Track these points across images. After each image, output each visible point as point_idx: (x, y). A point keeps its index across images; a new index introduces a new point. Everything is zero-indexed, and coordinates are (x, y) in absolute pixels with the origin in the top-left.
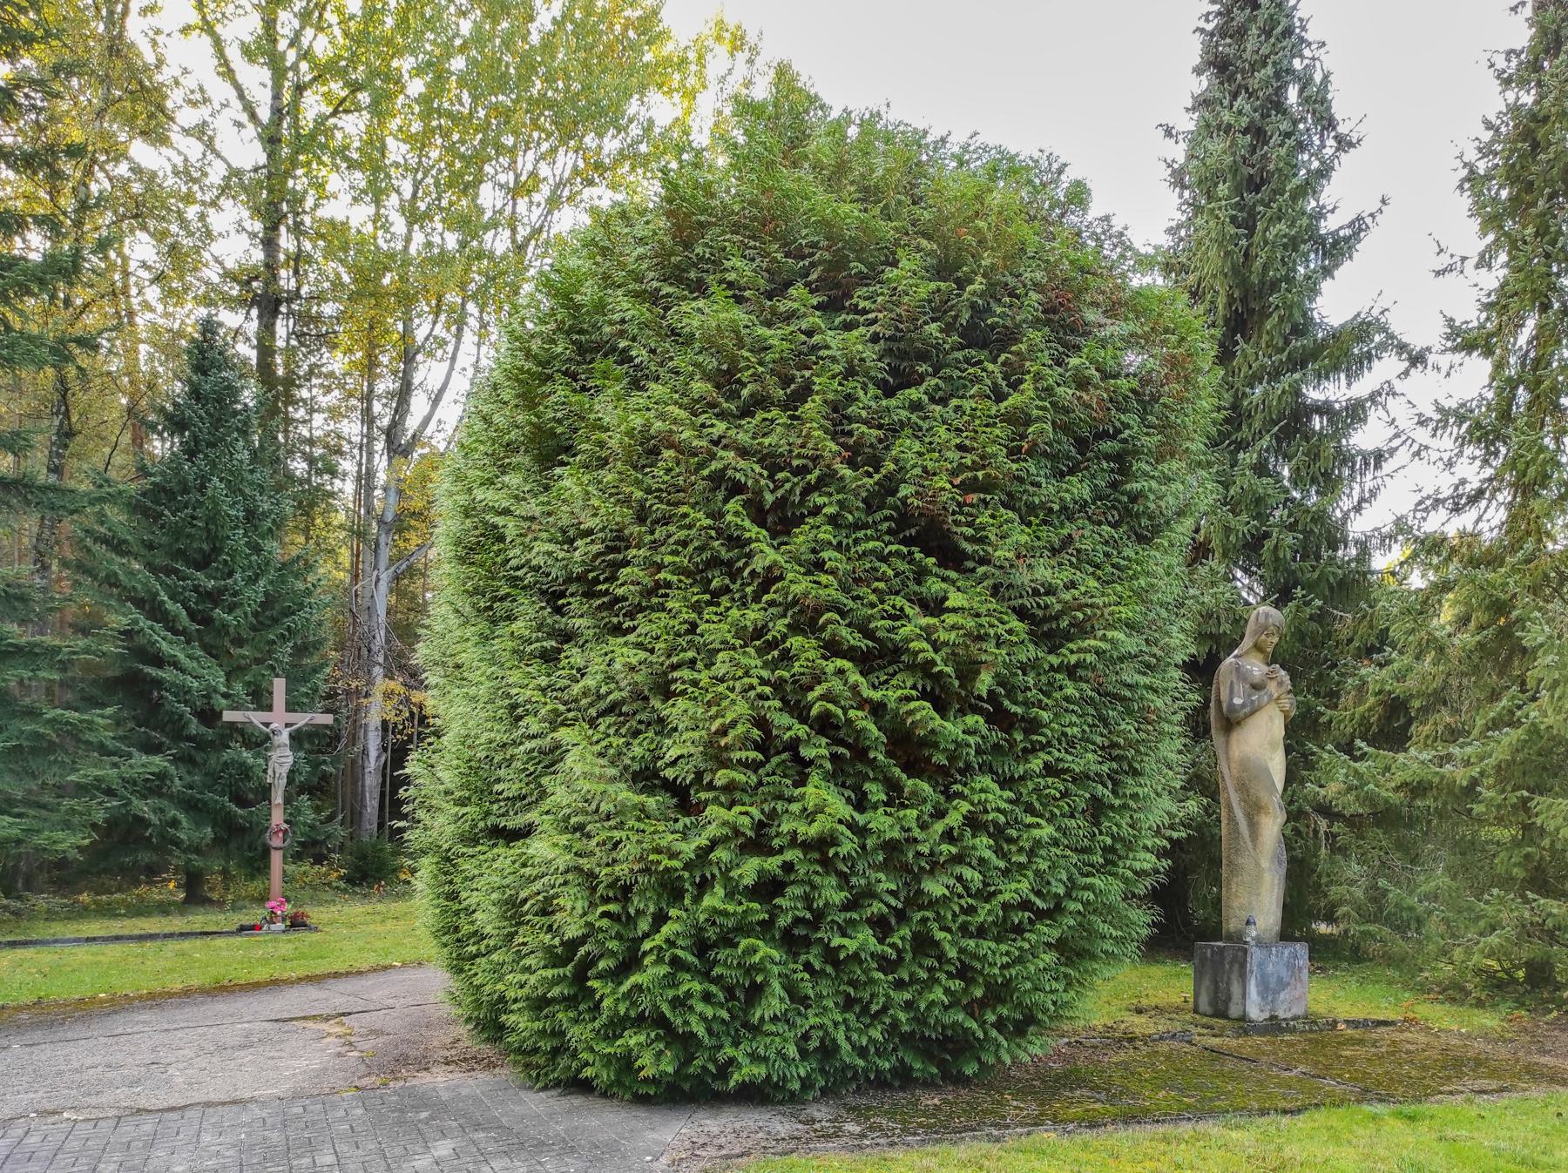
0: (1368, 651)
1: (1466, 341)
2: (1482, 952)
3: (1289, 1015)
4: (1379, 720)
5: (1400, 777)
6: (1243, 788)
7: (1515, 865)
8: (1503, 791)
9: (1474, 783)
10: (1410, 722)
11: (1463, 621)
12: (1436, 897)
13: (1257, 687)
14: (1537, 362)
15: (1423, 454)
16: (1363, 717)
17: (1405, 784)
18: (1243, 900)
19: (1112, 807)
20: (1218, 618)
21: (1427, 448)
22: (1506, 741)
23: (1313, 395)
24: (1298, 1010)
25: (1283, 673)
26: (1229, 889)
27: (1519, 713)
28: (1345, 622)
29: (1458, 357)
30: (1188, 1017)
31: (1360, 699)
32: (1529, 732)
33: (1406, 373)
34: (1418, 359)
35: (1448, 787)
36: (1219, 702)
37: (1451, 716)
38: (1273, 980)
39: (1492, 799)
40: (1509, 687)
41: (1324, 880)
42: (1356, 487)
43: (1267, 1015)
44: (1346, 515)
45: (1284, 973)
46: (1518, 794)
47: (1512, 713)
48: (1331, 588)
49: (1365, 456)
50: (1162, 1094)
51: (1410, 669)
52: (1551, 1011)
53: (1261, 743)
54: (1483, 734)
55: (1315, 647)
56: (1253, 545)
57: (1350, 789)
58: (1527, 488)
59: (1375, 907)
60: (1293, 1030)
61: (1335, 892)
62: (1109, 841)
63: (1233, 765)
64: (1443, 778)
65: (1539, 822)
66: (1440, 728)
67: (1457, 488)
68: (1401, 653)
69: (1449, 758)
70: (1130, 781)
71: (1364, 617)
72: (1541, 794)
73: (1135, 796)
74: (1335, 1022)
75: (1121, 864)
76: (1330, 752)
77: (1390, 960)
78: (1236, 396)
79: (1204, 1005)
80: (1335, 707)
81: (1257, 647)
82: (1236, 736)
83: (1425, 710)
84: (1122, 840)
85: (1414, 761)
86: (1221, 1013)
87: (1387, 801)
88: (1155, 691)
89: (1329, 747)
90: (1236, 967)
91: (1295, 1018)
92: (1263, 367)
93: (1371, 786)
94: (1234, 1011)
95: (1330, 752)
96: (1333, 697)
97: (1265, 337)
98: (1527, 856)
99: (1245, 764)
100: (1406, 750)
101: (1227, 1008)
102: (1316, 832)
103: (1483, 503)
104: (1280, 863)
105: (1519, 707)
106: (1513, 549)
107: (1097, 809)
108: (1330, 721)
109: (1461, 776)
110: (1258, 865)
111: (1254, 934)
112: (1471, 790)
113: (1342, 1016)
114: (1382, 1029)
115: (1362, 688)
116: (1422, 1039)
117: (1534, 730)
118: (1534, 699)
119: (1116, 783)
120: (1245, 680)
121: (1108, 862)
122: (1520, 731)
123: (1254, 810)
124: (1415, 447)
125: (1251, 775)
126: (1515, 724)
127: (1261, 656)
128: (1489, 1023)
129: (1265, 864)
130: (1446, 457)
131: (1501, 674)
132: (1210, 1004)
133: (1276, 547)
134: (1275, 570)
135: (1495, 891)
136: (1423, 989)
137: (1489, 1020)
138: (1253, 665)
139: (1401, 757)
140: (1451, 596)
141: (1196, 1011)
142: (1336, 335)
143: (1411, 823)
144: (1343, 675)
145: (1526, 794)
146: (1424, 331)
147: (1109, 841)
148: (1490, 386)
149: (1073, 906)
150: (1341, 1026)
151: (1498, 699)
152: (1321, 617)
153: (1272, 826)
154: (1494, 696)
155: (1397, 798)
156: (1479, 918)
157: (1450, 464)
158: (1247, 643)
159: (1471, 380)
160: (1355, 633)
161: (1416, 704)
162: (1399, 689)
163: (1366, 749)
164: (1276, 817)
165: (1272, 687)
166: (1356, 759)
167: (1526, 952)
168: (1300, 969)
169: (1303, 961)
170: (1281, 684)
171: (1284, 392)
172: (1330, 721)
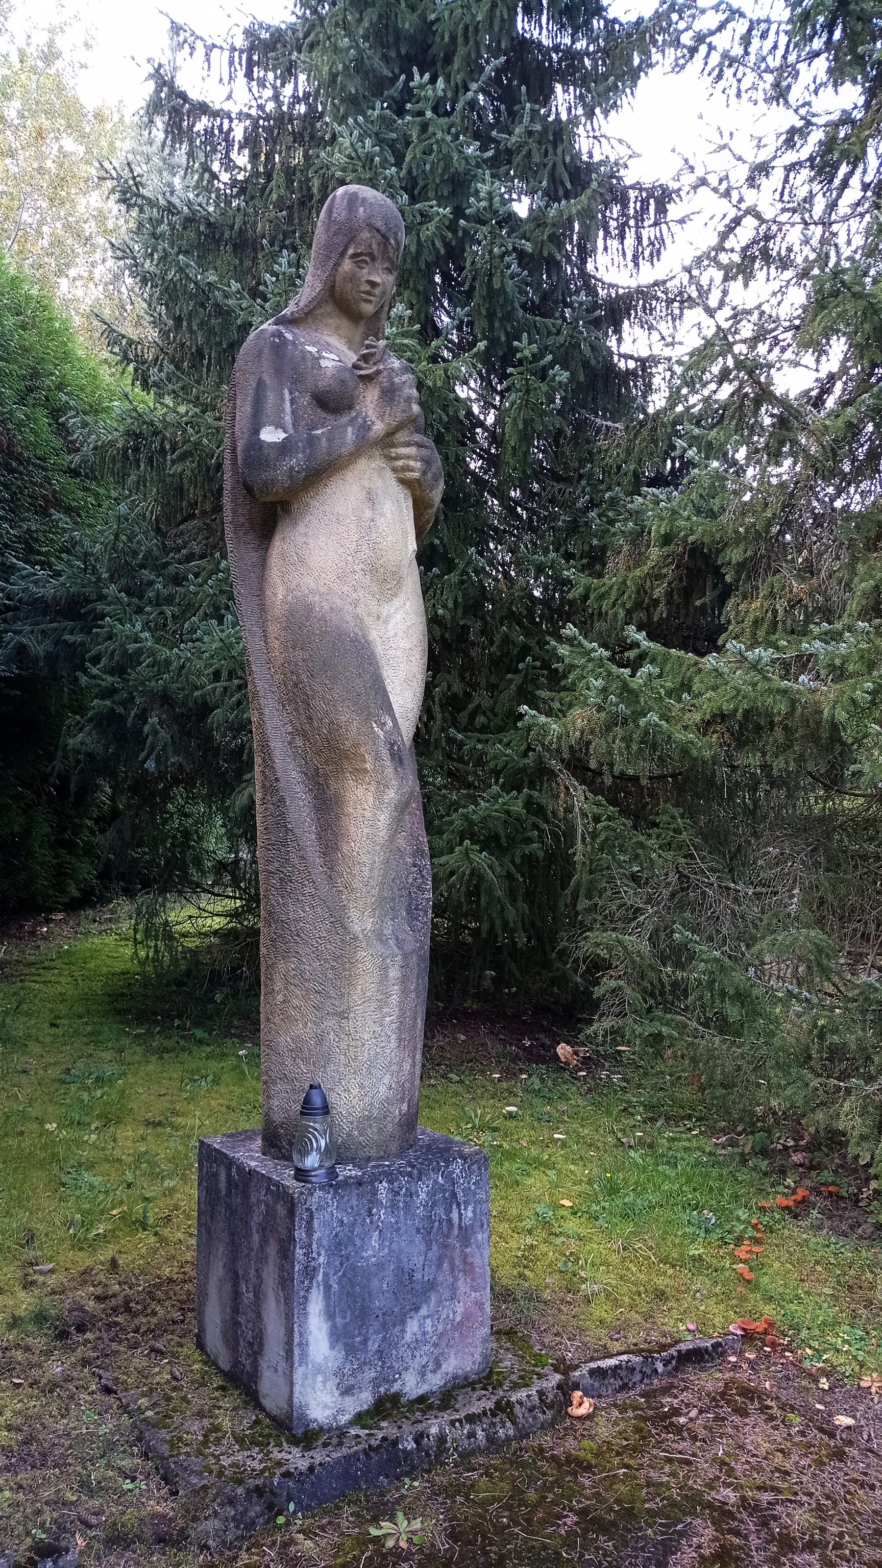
4: (669, 594)
5: (710, 702)
6: (297, 696)
13: (332, 402)
16: (641, 590)
17: (720, 717)
18: (303, 1030)
31: (639, 559)
38: (382, 1287)
41: (583, 904)
43: (365, 1399)
45: (416, 1254)
63: (274, 629)
69: (804, 662)
76: (570, 641)
82: (278, 545)
83: (750, 568)
85: (735, 669)
87: (685, 751)
90: (272, 1249)
99: (302, 622)
104: (412, 911)
108: (585, 597)
110: (339, 923)
120: (297, 382)
123: (328, 764)
125: (336, 654)
129: (361, 921)
139: (711, 660)
155: (707, 747)
161: (735, 555)
162: (698, 529)
163: (645, 644)
164: (382, 786)
165: (369, 401)
170: (389, 394)
172: (585, 597)
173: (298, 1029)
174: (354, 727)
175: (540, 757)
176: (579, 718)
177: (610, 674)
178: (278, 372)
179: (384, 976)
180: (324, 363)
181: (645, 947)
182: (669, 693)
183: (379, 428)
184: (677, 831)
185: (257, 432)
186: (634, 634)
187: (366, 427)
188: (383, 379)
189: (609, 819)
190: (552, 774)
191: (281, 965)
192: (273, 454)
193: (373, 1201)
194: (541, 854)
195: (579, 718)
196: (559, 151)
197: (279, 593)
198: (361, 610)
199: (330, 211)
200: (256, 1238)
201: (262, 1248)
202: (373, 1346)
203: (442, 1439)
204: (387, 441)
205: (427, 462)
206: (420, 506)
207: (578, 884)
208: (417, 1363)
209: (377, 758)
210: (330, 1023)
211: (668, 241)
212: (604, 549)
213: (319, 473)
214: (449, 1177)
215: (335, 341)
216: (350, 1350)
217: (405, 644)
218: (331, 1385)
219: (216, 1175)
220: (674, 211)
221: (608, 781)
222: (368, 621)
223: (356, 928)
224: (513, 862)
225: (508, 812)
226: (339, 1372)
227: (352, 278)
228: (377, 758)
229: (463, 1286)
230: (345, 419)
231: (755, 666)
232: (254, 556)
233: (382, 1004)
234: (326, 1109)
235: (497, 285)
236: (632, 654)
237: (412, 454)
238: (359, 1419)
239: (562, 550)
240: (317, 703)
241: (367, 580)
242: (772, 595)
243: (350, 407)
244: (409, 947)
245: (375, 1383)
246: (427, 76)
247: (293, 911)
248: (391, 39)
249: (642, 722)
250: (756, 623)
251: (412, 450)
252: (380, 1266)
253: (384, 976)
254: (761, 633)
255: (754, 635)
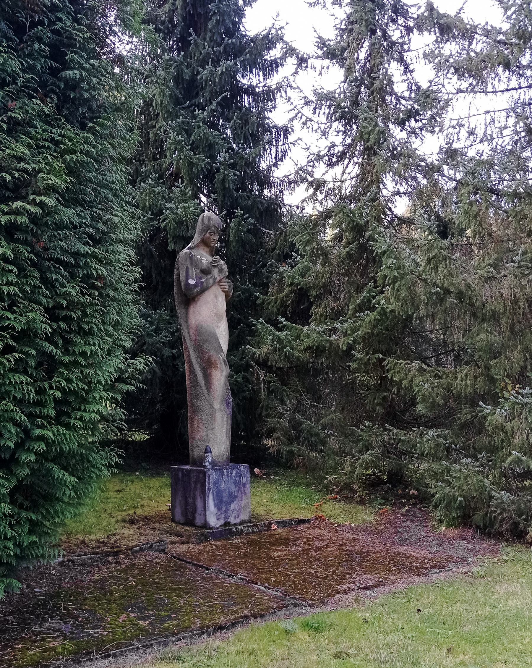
0: (285, 257)
1: (332, 54)
2: (359, 465)
3: (238, 521)
4: (292, 303)
5: (306, 342)
6: (199, 348)
7: (378, 404)
8: (367, 353)
9: (351, 347)
10: (311, 304)
11: (338, 238)
12: (332, 425)
13: (206, 272)
14: (371, 70)
15: (309, 124)
16: (282, 301)
17: (309, 348)
18: (203, 434)
19: (61, 363)
20: (187, 225)
21: (311, 120)
22: (367, 319)
23: (244, 81)
24: (245, 516)
25: (222, 262)
26: (192, 425)
27: (374, 301)
28: (269, 235)
29: (327, 62)
30: (165, 526)
31: (281, 290)
32: (380, 314)
33: (296, 72)
34: (302, 61)
35: (334, 349)
36: (179, 282)
37: (335, 302)
38: (225, 494)
39: (361, 359)
40: (367, 284)
42: (273, 149)
43: (222, 522)
44: (269, 167)
45: (233, 488)
46: (376, 356)
47: (370, 301)
48: (261, 213)
49: (278, 129)
50: (123, 617)
51: (308, 269)
52: (404, 505)
53: (210, 314)
54: (353, 315)
55: (252, 252)
56: (210, 175)
57: (275, 350)
58: (369, 152)
59: (295, 434)
60: (239, 533)
61: (271, 421)
62: (59, 394)
63: (192, 331)
64: (331, 343)
65: (390, 376)
66: (328, 310)
67: (329, 150)
68: (303, 257)
70: (79, 340)
71: (281, 234)
72: (390, 356)
73: (83, 354)
74: (270, 524)
75: (73, 415)
77: (311, 468)
78: (193, 73)
79: (179, 517)
80: (266, 294)
81: (205, 242)
82: (192, 309)
83: (318, 297)
84: (75, 393)
85: (313, 331)
86: (190, 522)
88: (100, 261)
89: (261, 320)
90: (199, 486)
91: (242, 523)
92: (208, 54)
93: (288, 348)
94: (199, 521)
95: (261, 323)
96: (265, 287)
97: (209, 34)
98: (384, 398)
99: (199, 331)
100: (309, 325)
101: (194, 518)
102: (258, 378)
103: (347, 161)
104: (228, 404)
105: (374, 297)
106: (364, 193)
107: (50, 366)
108: (263, 303)
109: (342, 342)
110: (211, 406)
111: (210, 460)
112: (347, 353)
113: (277, 517)
114: (302, 527)
115: (281, 281)
116: (326, 534)
117: (383, 312)
118: (382, 292)
119: (67, 343)
121: (60, 414)
122: (375, 313)
123: (208, 365)
124: (304, 119)
126: (372, 309)
127: (208, 250)
128: (368, 518)
129: (217, 405)
130: (322, 127)
131: (362, 276)
132: (182, 514)
133: (223, 179)
134: (224, 196)
135: (367, 423)
136: (327, 490)
137: (366, 516)
138: (202, 255)
140: (330, 222)
141: (173, 520)
142: (254, 40)
143: (317, 372)
144: (270, 272)
145: (381, 356)
146: (307, 46)
147: (59, 394)
148: (345, 82)
149: (24, 457)
150: (274, 527)
151: (362, 292)
152: (255, 232)
153: (220, 377)
154: (359, 289)
156: (358, 441)
157: (324, 133)
158: (197, 238)
159: (333, 78)
160: (276, 244)
161: (314, 293)
162: (302, 282)
164: (222, 371)
165: (215, 272)
166: (280, 330)
167: (385, 465)
168: (244, 485)
169: (246, 479)
170: (221, 271)
171: (222, 73)
172: (263, 303)
173: (201, 433)
174: (215, 356)
175: (247, 361)
176: (265, 349)
177: (274, 334)
178: (191, 264)
179: (223, 420)
180: (203, 261)
181: (286, 424)
182: (293, 340)
183: (218, 279)
184: (297, 386)
185: (187, 280)
186: (281, 319)
187: (215, 279)
188: (219, 267)
189: (274, 382)
190: (252, 367)
191: (196, 417)
192: (193, 287)
193: (223, 474)
194: (249, 396)
195: (265, 349)
196: (247, 128)
197: (193, 320)
198: (214, 325)
199: (203, 220)
200: (193, 485)
201: (195, 487)
202: (224, 509)
203: (241, 530)
204: (220, 281)
205: (230, 286)
206: (227, 296)
207: (262, 407)
208: (234, 515)
209: (221, 364)
210: (210, 431)
211: (289, 151)
212: (268, 283)
213: (204, 290)
214: (240, 470)
215: (204, 253)
216: (219, 509)
217: (224, 333)
218: (215, 517)
219: (178, 475)
220: (291, 138)
221: (275, 369)
222: (216, 328)
223: (215, 407)
224: (239, 399)
225: (237, 381)
226: (216, 514)
227: (209, 238)
228: (221, 364)
229: (244, 498)
230: (209, 277)
231: (318, 333)
232: (183, 311)
233: (223, 427)
234: (211, 452)
235: (227, 186)
236: (280, 326)
237: (226, 284)
238: (221, 526)
239: (252, 282)
240: (205, 350)
241: (215, 318)
242: (325, 307)
243: (210, 273)
244: (228, 412)
245: (225, 518)
246: (201, 111)
247: (199, 403)
248: (180, 81)
249: (285, 350)
250: (321, 316)
251: (226, 284)
252: (225, 490)
253: (223, 420)
254: (323, 319)
255: (320, 320)
